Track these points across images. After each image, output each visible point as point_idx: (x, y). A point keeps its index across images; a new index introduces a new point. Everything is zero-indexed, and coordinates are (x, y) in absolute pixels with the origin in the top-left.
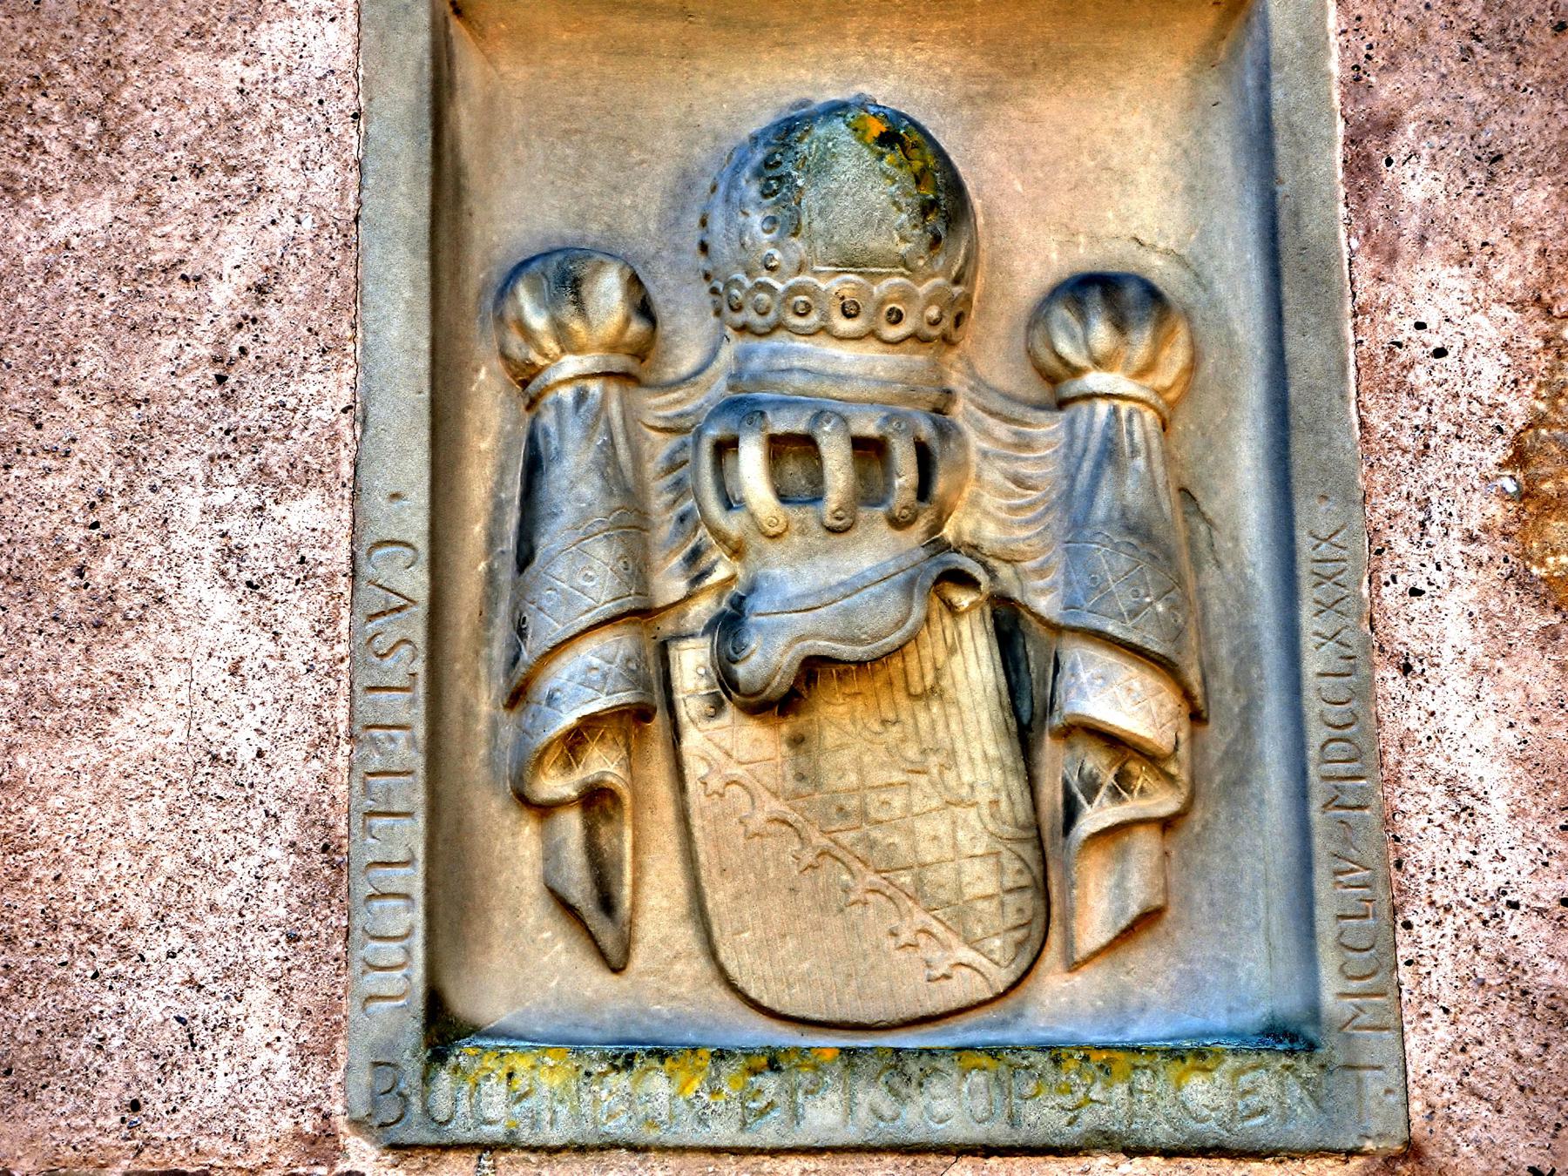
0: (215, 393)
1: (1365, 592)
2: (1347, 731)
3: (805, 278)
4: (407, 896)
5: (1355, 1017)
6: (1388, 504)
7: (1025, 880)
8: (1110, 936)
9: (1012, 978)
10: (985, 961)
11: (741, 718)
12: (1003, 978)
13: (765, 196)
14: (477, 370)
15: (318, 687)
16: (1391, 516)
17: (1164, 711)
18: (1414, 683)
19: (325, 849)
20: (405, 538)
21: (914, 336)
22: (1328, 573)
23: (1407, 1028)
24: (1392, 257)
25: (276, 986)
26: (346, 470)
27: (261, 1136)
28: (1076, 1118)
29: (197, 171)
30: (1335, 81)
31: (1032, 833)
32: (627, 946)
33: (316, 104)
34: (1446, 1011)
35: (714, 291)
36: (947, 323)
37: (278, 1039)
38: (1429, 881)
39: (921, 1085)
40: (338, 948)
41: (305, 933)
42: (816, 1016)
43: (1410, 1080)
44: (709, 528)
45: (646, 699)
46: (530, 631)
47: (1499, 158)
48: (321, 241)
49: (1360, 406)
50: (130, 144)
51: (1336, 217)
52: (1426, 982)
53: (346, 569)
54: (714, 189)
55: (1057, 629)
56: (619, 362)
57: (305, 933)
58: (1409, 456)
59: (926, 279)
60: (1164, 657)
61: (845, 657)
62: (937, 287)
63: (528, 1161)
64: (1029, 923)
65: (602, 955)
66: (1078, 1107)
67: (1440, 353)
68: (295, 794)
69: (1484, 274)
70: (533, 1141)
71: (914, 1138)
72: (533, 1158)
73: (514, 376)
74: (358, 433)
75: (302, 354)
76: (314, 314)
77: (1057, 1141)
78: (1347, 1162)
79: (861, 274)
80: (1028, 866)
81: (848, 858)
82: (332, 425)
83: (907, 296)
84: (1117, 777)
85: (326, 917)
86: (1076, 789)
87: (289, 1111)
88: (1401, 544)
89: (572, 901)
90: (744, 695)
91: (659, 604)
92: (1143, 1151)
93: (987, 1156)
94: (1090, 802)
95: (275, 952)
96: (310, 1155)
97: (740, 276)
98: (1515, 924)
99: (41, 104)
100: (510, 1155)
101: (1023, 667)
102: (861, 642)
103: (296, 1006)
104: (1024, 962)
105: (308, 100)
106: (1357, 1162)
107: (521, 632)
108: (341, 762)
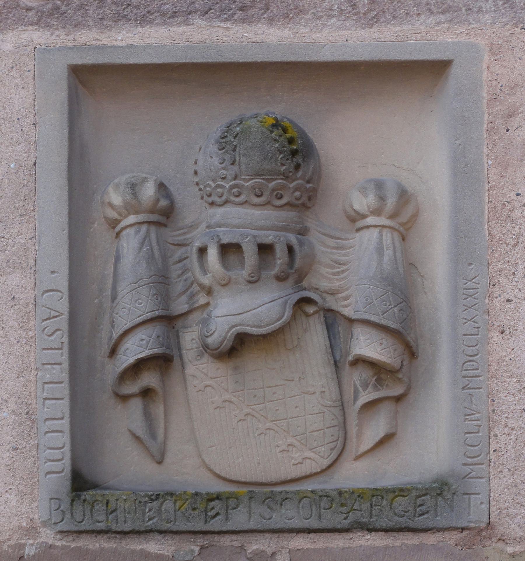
1: (487, 301)
2: (474, 358)
3: (237, 182)
4: (61, 432)
5: (471, 473)
7: (335, 423)
9: (329, 463)
10: (317, 456)
11: (210, 360)
12: (326, 462)
13: (220, 150)
14: (94, 223)
15: (22, 348)
16: (501, 270)
17: (396, 352)
18: (506, 337)
19: (27, 413)
20: (58, 288)
22: (471, 294)
23: (492, 477)
24: (506, 167)
25: (9, 468)
26: (32, 262)
27: (5, 528)
28: (347, 517)
30: (485, 100)
31: (339, 403)
33: (16, 120)
34: (509, 470)
35: (200, 190)
36: (304, 199)
37: (11, 489)
38: (506, 417)
39: (281, 505)
40: (34, 452)
41: (20, 447)
42: (244, 480)
43: (491, 498)
44: (197, 283)
45: (168, 351)
46: (116, 326)
48: (19, 173)
49: (489, 226)
51: (482, 152)
52: (502, 458)
53: (33, 302)
54: (200, 149)
55: (351, 321)
56: (154, 217)
57: (20, 447)
58: (510, 246)
59: (294, 181)
60: (396, 330)
61: (254, 333)
62: (299, 184)
63: (116, 537)
64: (337, 440)
66: (349, 512)
68: (14, 391)
70: (118, 529)
71: (278, 526)
72: (118, 536)
73: (110, 225)
74: (37, 247)
75: (11, 217)
76: (17, 202)
77: (339, 527)
78: (462, 532)
79: (263, 179)
80: (337, 417)
81: (257, 415)
82: (25, 245)
83: (283, 187)
84: (376, 380)
85: (29, 440)
86: (358, 386)
87: (17, 518)
88: (504, 281)
89: (137, 435)
90: (212, 350)
91: (176, 314)
93: (309, 533)
94: (364, 390)
95: (8, 454)
96: (26, 535)
97: (211, 183)
100: (108, 535)
101: (337, 337)
102: (261, 327)
103: (17, 476)
104: (333, 456)
105: (12, 119)
106: (465, 533)
107: (113, 326)
108: (32, 378)
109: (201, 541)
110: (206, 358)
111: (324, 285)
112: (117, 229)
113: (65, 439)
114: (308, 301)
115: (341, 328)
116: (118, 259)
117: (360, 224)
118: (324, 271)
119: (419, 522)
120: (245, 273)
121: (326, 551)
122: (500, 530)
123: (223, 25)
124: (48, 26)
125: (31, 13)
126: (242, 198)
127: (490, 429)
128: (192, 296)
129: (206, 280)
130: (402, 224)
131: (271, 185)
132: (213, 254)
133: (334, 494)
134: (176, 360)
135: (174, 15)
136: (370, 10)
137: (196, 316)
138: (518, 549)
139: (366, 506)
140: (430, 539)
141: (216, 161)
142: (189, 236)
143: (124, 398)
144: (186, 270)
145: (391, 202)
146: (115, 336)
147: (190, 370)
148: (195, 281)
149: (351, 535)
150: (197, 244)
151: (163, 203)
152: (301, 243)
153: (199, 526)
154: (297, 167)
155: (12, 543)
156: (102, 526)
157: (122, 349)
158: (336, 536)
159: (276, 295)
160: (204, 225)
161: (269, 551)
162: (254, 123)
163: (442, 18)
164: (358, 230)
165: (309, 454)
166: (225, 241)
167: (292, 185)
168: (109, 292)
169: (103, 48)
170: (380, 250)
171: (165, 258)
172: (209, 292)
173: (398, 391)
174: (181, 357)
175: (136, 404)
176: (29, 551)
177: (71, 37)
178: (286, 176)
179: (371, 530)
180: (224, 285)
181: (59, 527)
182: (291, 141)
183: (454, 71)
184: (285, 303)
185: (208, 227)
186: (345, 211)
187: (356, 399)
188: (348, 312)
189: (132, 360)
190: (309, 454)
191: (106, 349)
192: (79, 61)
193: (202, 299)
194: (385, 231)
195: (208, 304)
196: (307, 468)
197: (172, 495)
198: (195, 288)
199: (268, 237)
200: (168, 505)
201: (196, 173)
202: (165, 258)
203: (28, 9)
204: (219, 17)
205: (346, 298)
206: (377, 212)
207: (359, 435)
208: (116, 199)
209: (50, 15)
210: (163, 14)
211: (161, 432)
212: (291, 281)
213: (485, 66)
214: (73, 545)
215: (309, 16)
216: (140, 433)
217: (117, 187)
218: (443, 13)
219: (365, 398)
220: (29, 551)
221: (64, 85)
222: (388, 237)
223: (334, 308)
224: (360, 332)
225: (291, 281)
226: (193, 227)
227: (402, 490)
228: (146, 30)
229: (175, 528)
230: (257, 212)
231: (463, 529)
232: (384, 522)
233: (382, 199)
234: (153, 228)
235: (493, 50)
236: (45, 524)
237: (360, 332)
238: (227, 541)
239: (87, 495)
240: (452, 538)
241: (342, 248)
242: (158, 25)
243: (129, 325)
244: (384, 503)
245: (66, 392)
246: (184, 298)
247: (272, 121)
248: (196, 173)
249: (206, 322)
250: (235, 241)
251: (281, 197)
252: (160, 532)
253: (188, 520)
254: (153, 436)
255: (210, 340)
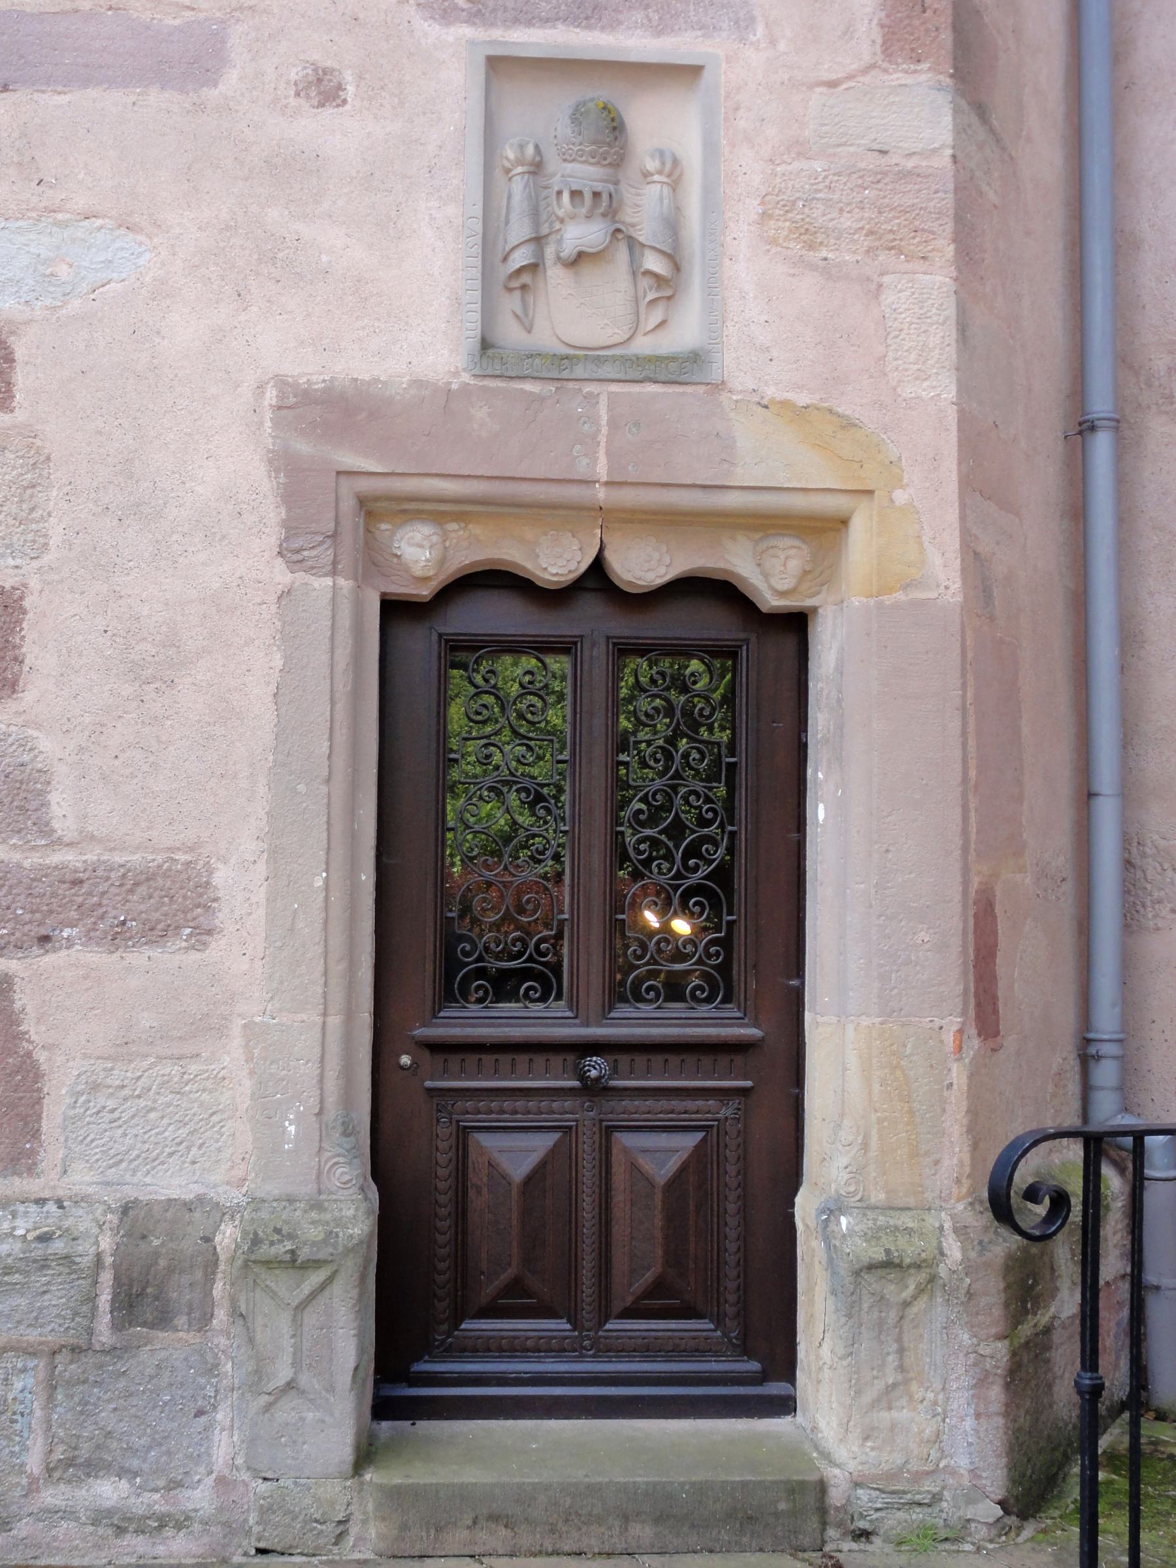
0: (429, 175)
3: (582, 147)
6: (730, 214)
8: (427, 1427)
12: (627, 337)
16: (730, 218)
21: (610, 164)
26: (461, 197)
29: (424, 114)
32: (531, 326)
40: (459, 324)
47: (763, 120)
50: (407, 105)
55: (643, 245)
56: (532, 169)
65: (525, 328)
67: (745, 174)
69: (757, 152)
71: (602, 377)
83: (607, 152)
88: (732, 225)
92: (658, 382)
98: (753, 327)
99: (384, 94)
107: (506, 242)
109: (559, 384)
110: (559, 266)
111: (629, 220)
112: (510, 175)
113: (478, 316)
114: (618, 230)
115: (637, 249)
116: (509, 197)
117: (649, 179)
118: (629, 211)
119: (683, 378)
120: (584, 211)
121: (629, 393)
122: (729, 385)
123: (575, 30)
124: (474, 24)
125: (464, 14)
126: (584, 158)
127: (724, 322)
128: (551, 224)
129: (561, 213)
130: (673, 181)
131: (601, 150)
132: (566, 196)
133: (634, 358)
134: (541, 266)
135: (547, 20)
136: (659, 25)
137: (553, 238)
138: (739, 397)
139: (652, 367)
140: (689, 389)
141: (569, 131)
142: (550, 181)
143: (510, 290)
144: (548, 205)
145: (668, 166)
146: (507, 249)
147: (549, 273)
148: (554, 213)
149: (644, 385)
150: (556, 189)
151: (538, 159)
152: (616, 190)
153: (556, 375)
154: (616, 138)
155: (444, 381)
156: (498, 372)
157: (511, 258)
158: (635, 384)
159: (601, 226)
160: (559, 175)
161: (596, 392)
162: (591, 105)
163: (699, 33)
164: (648, 183)
165: (617, 331)
166: (573, 189)
167: (613, 151)
168: (503, 218)
169: (506, 43)
170: (661, 199)
171: (537, 196)
172: (562, 221)
173: (669, 293)
174: (544, 264)
175: (517, 294)
176: (454, 387)
177: (487, 34)
178: (609, 145)
179: (656, 382)
180: (572, 218)
181: (473, 372)
182: (613, 120)
183: (706, 74)
184: (607, 232)
185: (563, 176)
186: (641, 170)
187: (645, 297)
188: (641, 239)
189: (518, 266)
190: (617, 331)
191: (500, 256)
192: (492, 52)
193: (557, 226)
194: (664, 186)
195: (560, 230)
196: (617, 339)
197: (540, 355)
198: (553, 217)
199: (599, 187)
200: (537, 361)
201: (555, 137)
202: (537, 196)
203: (463, 10)
204: (572, 24)
205: (640, 230)
206: (660, 172)
207: (647, 319)
208: (511, 154)
209: (476, 16)
210: (541, 20)
211: (531, 312)
212: (610, 216)
213: (723, 71)
214: (481, 384)
215: (624, 27)
216: (519, 312)
217: (511, 146)
218: (700, 29)
219: (651, 296)
220: (454, 387)
221: (483, 70)
222: (666, 190)
223: (634, 235)
224: (647, 252)
225: (610, 216)
226: (553, 175)
227: (673, 358)
228: (531, 31)
229: (541, 376)
230: (592, 169)
231: (708, 384)
232: (663, 378)
233: (663, 163)
234: (531, 177)
235: (728, 59)
236: (464, 370)
237: (647, 252)
238: (571, 385)
239: (490, 352)
240: (701, 389)
241: (639, 195)
242: (539, 28)
243: (516, 243)
244: (663, 366)
245: (479, 287)
246: (547, 225)
247: (602, 105)
248: (555, 137)
249: (560, 242)
250: (578, 189)
251: (605, 159)
252: (533, 378)
253: (549, 370)
254: (527, 315)
255: (562, 255)
